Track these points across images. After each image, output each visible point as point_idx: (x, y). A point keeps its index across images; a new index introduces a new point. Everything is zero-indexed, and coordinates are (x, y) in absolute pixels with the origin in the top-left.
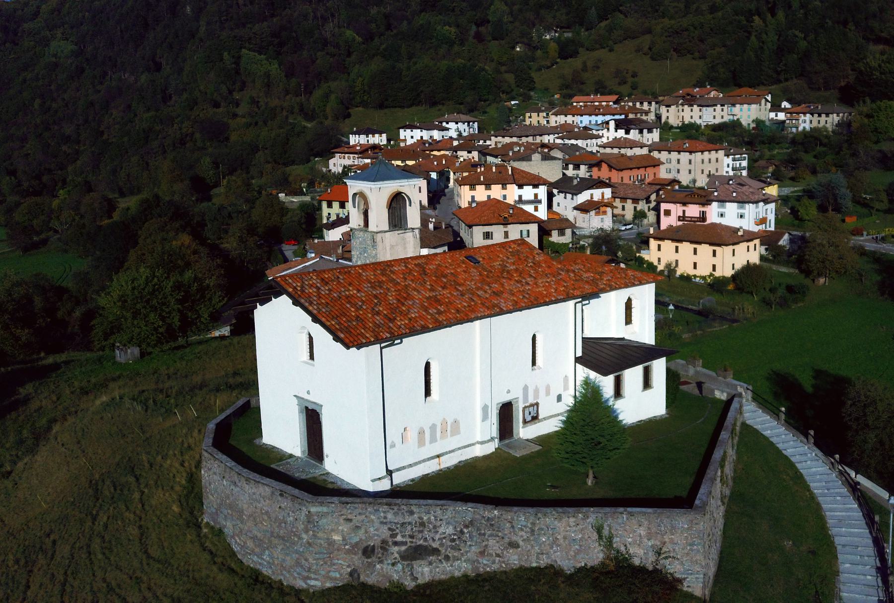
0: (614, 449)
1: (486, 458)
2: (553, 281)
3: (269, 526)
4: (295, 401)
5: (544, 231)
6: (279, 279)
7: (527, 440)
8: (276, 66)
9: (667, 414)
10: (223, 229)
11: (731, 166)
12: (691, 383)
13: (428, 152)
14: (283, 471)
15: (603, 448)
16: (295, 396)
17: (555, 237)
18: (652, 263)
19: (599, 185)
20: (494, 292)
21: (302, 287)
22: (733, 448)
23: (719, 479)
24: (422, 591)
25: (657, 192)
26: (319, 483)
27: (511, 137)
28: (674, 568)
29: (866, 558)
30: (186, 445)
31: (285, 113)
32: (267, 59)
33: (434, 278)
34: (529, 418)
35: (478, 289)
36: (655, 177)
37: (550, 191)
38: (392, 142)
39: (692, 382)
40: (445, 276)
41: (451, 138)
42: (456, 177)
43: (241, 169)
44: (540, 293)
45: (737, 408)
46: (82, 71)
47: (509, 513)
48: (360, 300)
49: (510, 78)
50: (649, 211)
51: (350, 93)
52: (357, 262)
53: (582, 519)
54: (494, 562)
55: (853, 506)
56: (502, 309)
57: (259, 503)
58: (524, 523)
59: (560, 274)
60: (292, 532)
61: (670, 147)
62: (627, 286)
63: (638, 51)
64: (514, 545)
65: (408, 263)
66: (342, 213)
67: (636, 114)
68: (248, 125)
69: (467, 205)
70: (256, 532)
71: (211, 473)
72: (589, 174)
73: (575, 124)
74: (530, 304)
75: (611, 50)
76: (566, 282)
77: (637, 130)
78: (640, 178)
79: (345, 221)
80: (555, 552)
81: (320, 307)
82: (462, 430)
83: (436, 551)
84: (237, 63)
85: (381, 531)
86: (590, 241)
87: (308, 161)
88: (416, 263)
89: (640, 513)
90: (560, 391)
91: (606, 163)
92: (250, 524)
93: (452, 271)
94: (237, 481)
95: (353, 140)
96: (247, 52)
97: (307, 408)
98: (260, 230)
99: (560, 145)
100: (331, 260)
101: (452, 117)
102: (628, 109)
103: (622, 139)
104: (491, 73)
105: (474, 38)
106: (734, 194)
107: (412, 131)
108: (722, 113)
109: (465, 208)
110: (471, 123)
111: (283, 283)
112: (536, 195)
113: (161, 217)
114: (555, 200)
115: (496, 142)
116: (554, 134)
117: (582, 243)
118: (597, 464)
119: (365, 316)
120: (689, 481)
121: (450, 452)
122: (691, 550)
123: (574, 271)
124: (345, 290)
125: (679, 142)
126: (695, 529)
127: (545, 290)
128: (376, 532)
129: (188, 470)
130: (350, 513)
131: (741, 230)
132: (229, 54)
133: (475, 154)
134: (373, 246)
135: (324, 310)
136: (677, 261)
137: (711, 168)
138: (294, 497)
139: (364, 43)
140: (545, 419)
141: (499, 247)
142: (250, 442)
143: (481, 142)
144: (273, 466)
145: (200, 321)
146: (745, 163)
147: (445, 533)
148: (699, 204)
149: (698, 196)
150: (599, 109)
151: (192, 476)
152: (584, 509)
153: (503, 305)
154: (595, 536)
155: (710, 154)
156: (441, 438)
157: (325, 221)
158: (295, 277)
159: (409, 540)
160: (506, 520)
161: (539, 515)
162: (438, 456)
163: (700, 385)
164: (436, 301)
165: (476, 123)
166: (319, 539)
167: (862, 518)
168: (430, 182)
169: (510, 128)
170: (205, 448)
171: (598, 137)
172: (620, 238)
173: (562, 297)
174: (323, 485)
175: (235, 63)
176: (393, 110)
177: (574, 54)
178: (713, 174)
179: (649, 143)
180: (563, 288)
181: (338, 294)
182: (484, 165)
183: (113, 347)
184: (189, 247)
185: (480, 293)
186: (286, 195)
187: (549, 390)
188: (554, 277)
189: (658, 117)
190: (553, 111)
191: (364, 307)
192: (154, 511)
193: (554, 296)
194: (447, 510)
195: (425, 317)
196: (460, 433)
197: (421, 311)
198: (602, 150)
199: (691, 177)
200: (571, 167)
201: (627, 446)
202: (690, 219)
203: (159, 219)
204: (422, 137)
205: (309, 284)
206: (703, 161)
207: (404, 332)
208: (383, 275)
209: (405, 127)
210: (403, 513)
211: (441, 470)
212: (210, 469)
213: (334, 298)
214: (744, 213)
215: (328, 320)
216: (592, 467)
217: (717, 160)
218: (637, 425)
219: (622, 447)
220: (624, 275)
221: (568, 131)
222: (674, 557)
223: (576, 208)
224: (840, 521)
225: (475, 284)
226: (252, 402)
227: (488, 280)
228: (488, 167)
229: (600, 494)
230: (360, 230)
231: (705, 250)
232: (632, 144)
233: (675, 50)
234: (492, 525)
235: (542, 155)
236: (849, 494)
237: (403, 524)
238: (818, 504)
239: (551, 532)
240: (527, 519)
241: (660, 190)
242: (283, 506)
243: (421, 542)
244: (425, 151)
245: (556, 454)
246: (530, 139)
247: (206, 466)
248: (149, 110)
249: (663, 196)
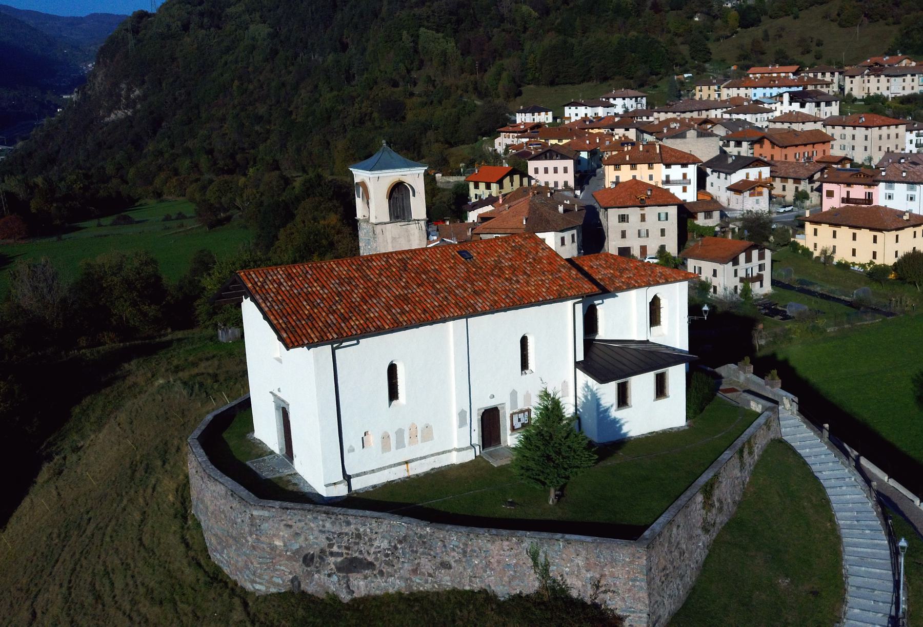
1: (462, 466)
8: (453, 44)
11: (914, 142)
14: (254, 469)
16: (271, 392)
17: (701, 220)
18: (808, 249)
19: (756, 163)
24: (356, 605)
28: (615, 604)
29: (881, 604)
31: (459, 92)
32: (444, 38)
35: (458, 287)
36: (824, 154)
38: (558, 121)
39: (739, 389)
44: (529, 292)
46: (276, 52)
47: (443, 532)
49: (685, 50)
51: (522, 71)
53: (517, 544)
54: (426, 582)
55: (882, 542)
58: (456, 543)
63: (825, 17)
64: (446, 566)
67: (816, 86)
68: (424, 104)
72: (751, 151)
75: (796, 17)
77: (814, 104)
78: (806, 155)
80: (489, 576)
83: (371, 565)
84: (415, 42)
85: (319, 539)
86: (739, 224)
87: (476, 140)
89: (576, 541)
95: (520, 118)
96: (426, 30)
101: (619, 92)
102: (808, 80)
104: (664, 45)
105: (651, 9)
106: (904, 174)
108: (913, 84)
110: (639, 99)
111: (245, 278)
112: (685, 175)
114: (709, 180)
117: (731, 226)
121: (421, 458)
122: (634, 586)
130: (290, 519)
131: (907, 214)
132: (408, 33)
136: (834, 247)
139: (540, 18)
144: (248, 463)
147: (380, 547)
148: (865, 185)
150: (774, 81)
154: (530, 562)
159: (345, 551)
161: (472, 536)
162: (407, 463)
165: (644, 98)
166: (262, 543)
167: (889, 558)
168: (578, 162)
171: (770, 111)
175: (413, 41)
176: (563, 87)
177: (756, 22)
178: (893, 152)
179: (825, 117)
183: (216, 327)
184: (333, 228)
188: (552, 274)
189: (842, 88)
190: (725, 84)
194: (382, 523)
198: (772, 126)
199: (866, 155)
200: (732, 143)
204: (586, 115)
206: (889, 136)
209: (570, 105)
210: (340, 524)
221: (737, 105)
222: (614, 592)
223: (729, 189)
224: (862, 558)
231: (865, 235)
232: (805, 119)
233: (866, 15)
234: (424, 543)
235: (698, 132)
236: (882, 528)
237: (340, 534)
238: (839, 538)
240: (459, 540)
242: (234, 506)
243: (357, 554)
246: (695, 115)
248: (332, 90)
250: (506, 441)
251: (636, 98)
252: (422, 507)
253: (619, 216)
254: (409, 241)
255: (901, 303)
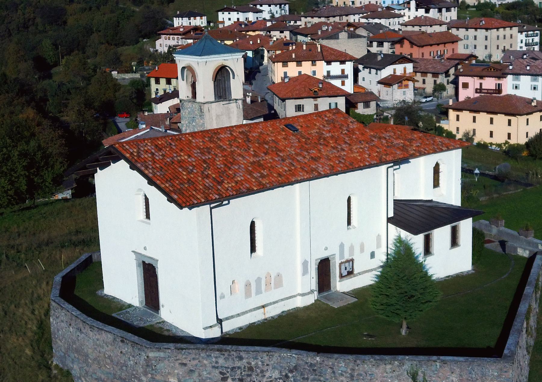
0: (427, 302)
1: (306, 308)
2: (366, 147)
3: (112, 369)
4: (133, 256)
5: (351, 104)
6: (117, 145)
7: (344, 293)
9: (473, 270)
10: (63, 103)
11: (524, 42)
12: (493, 242)
13: (244, 33)
14: (123, 319)
15: (416, 301)
16: (133, 251)
17: (361, 109)
19: (401, 60)
20: (312, 158)
21: (138, 152)
22: (536, 301)
23: (524, 330)
25: (456, 66)
26: (156, 331)
27: (320, 17)
30: (35, 295)
33: (257, 145)
34: (345, 273)
35: (297, 154)
36: (453, 52)
37: (355, 67)
38: (212, 24)
40: (267, 143)
41: (264, 19)
42: (270, 55)
43: (78, 50)
44: (355, 158)
45: (539, 265)
47: (331, 360)
48: (191, 164)
50: (448, 84)
52: (186, 130)
53: (398, 366)
56: (320, 173)
57: (103, 348)
58: (345, 369)
59: (373, 141)
60: (133, 374)
61: (467, 25)
62: (435, 152)
65: (233, 131)
66: (170, 89)
68: (83, 10)
69: (280, 81)
70: (100, 374)
71: (58, 320)
73: (378, 4)
74: (346, 168)
76: (378, 148)
77: (437, 10)
78: (439, 53)
79: (175, 94)
81: (155, 171)
82: (284, 283)
85: (213, 374)
86: (393, 112)
87: (137, 42)
88: (241, 131)
90: (374, 249)
91: (408, 40)
92: (95, 366)
93: (273, 138)
94: (82, 329)
95: (177, 22)
97: (144, 262)
98: (97, 104)
99: (365, 24)
100: (160, 131)
103: (423, 17)
107: (229, 13)
109: (279, 84)
110: (283, 6)
112: (343, 71)
113: (8, 93)
114: (361, 75)
115: (306, 23)
116: (359, 14)
117: (385, 114)
118: (410, 315)
119: (196, 179)
120: (497, 332)
121: (274, 303)
123: (385, 138)
124: (177, 156)
125: (476, 20)
126: (504, 376)
127: (359, 156)
128: (208, 376)
129: (39, 318)
131: (535, 101)
133: (287, 34)
134: (200, 116)
135: (158, 174)
136: (474, 131)
137: (503, 44)
138: (134, 343)
140: (359, 274)
141: (316, 116)
142: (93, 293)
143: (292, 23)
144: (114, 315)
145: (45, 185)
146: (537, 39)
147: (271, 377)
148: (495, 77)
149: (494, 70)
151: (42, 323)
152: (400, 357)
153: (320, 169)
155: (504, 30)
156: (266, 290)
157: (153, 96)
158: (132, 144)
160: (327, 366)
161: (358, 362)
162: (263, 307)
163: (503, 244)
164: (258, 165)
165: (287, 5)
169: (319, 9)
170: (53, 298)
171: (400, 16)
172: (421, 110)
173: (375, 162)
174: (159, 333)
178: (508, 50)
180: (376, 154)
181: (171, 159)
182: (295, 43)
184: (33, 120)
185: (299, 158)
186: (118, 73)
187: (364, 247)
188: (367, 143)
191: (195, 171)
192: (9, 354)
193: (368, 161)
195: (249, 180)
196: (283, 286)
197: (246, 175)
198: (404, 28)
199: (487, 52)
200: (375, 44)
201: (438, 299)
202: (486, 91)
203: (7, 95)
204: (238, 19)
205: (144, 149)
207: (231, 193)
208: (211, 141)
209: (223, 10)
211: (266, 319)
212: (57, 318)
213: (168, 163)
214: (537, 86)
215: (162, 183)
216: (405, 318)
217: (511, 36)
218: (445, 280)
219: (434, 300)
220: (432, 142)
225: (295, 150)
226: (93, 257)
227: (307, 146)
228: (299, 45)
229: (413, 343)
230: (189, 101)
231: (501, 119)
232: (432, 23)
234: (314, 370)
235: (349, 34)
237: (233, 369)
239: (369, 378)
241: (458, 64)
242: (124, 351)
244: (241, 31)
245: (372, 306)
246: (337, 19)
247: (54, 314)
249: (461, 70)
250: (336, 287)
251: (280, 5)
252: (293, 342)
253: (296, 106)
254: (229, 118)
255: (537, 175)
